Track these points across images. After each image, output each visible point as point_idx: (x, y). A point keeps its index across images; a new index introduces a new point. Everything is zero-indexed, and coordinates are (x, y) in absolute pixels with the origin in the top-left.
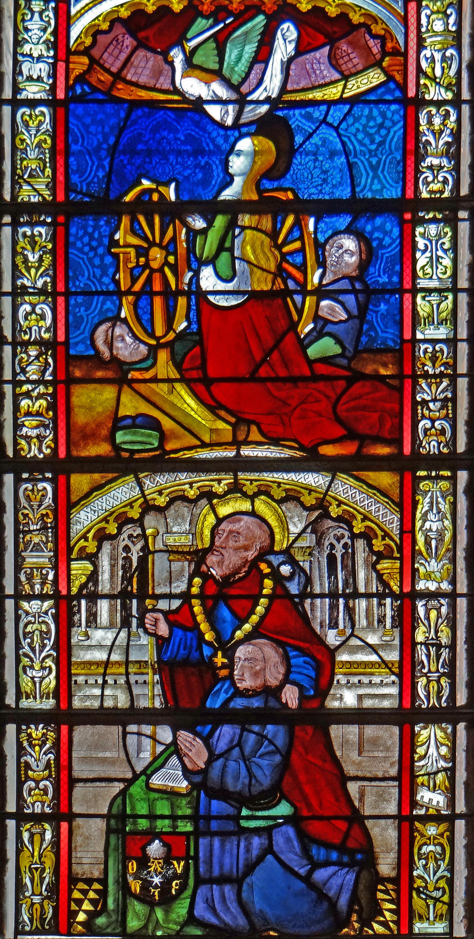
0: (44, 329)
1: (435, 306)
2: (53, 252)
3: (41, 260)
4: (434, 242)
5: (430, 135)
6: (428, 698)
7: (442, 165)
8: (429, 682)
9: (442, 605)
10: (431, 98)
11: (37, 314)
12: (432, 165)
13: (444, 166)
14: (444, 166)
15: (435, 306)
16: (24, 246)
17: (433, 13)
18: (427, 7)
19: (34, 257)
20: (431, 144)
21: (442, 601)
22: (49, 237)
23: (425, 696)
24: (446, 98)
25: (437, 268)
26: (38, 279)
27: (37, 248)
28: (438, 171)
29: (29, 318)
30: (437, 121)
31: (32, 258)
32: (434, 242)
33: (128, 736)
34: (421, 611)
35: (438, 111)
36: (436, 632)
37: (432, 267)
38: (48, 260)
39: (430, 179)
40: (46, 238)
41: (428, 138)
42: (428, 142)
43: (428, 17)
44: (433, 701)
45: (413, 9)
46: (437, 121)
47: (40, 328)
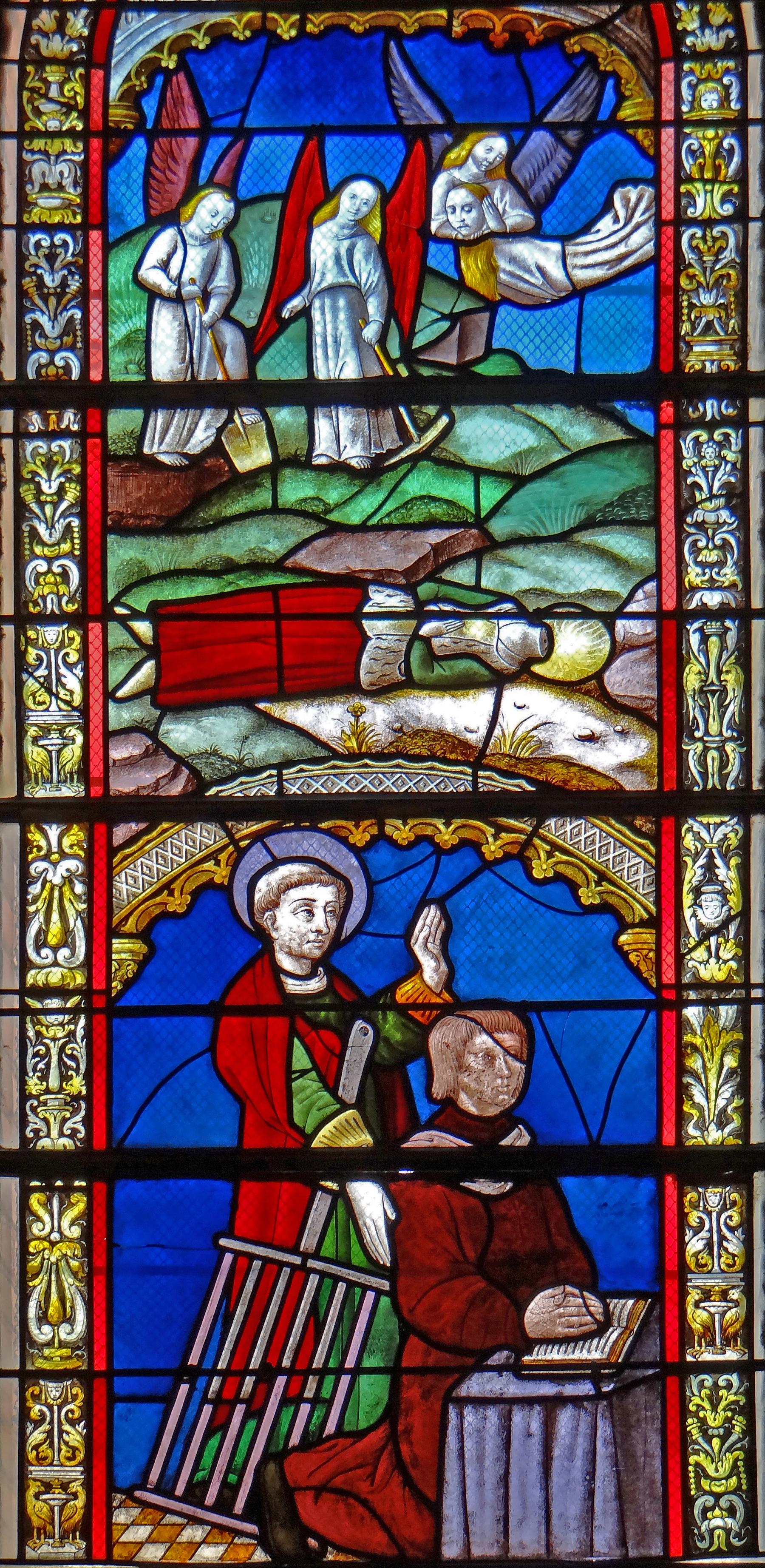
0: (65, 599)
1: (717, 1317)
2: (82, 480)
3: (61, 492)
4: (714, 1215)
5: (701, 474)
6: (704, 775)
7: (721, 521)
8: (706, 749)
9: (727, 629)
10: (698, 214)
11: (54, 574)
12: (704, 522)
13: (725, 522)
14: (725, 522)
15: (717, 1317)
16: (34, 468)
17: (700, 81)
18: (692, 72)
19: (50, 487)
20: (700, 489)
21: (728, 623)
22: (75, 456)
23: (699, 772)
24: (725, 214)
25: (720, 1256)
26: (58, 521)
27: (56, 471)
28: (715, 530)
29: (41, 580)
30: (709, 451)
31: (49, 488)
32: (714, 1215)
33: (210, 1021)
34: (695, 639)
35: (711, 439)
36: (719, 672)
37: (711, 1254)
38: (72, 493)
39: (701, 544)
40: (71, 457)
41: (697, 479)
42: (696, 486)
43: (693, 87)
44: (713, 782)
45: (670, 558)
46: (709, 451)
47: (60, 598)
